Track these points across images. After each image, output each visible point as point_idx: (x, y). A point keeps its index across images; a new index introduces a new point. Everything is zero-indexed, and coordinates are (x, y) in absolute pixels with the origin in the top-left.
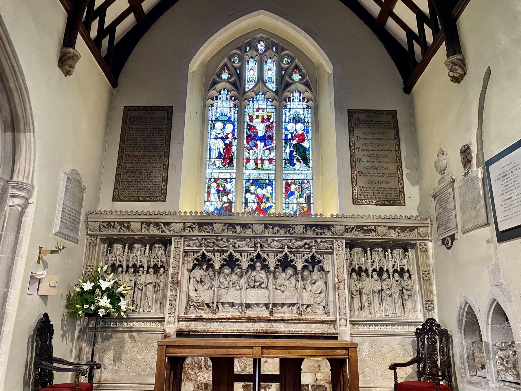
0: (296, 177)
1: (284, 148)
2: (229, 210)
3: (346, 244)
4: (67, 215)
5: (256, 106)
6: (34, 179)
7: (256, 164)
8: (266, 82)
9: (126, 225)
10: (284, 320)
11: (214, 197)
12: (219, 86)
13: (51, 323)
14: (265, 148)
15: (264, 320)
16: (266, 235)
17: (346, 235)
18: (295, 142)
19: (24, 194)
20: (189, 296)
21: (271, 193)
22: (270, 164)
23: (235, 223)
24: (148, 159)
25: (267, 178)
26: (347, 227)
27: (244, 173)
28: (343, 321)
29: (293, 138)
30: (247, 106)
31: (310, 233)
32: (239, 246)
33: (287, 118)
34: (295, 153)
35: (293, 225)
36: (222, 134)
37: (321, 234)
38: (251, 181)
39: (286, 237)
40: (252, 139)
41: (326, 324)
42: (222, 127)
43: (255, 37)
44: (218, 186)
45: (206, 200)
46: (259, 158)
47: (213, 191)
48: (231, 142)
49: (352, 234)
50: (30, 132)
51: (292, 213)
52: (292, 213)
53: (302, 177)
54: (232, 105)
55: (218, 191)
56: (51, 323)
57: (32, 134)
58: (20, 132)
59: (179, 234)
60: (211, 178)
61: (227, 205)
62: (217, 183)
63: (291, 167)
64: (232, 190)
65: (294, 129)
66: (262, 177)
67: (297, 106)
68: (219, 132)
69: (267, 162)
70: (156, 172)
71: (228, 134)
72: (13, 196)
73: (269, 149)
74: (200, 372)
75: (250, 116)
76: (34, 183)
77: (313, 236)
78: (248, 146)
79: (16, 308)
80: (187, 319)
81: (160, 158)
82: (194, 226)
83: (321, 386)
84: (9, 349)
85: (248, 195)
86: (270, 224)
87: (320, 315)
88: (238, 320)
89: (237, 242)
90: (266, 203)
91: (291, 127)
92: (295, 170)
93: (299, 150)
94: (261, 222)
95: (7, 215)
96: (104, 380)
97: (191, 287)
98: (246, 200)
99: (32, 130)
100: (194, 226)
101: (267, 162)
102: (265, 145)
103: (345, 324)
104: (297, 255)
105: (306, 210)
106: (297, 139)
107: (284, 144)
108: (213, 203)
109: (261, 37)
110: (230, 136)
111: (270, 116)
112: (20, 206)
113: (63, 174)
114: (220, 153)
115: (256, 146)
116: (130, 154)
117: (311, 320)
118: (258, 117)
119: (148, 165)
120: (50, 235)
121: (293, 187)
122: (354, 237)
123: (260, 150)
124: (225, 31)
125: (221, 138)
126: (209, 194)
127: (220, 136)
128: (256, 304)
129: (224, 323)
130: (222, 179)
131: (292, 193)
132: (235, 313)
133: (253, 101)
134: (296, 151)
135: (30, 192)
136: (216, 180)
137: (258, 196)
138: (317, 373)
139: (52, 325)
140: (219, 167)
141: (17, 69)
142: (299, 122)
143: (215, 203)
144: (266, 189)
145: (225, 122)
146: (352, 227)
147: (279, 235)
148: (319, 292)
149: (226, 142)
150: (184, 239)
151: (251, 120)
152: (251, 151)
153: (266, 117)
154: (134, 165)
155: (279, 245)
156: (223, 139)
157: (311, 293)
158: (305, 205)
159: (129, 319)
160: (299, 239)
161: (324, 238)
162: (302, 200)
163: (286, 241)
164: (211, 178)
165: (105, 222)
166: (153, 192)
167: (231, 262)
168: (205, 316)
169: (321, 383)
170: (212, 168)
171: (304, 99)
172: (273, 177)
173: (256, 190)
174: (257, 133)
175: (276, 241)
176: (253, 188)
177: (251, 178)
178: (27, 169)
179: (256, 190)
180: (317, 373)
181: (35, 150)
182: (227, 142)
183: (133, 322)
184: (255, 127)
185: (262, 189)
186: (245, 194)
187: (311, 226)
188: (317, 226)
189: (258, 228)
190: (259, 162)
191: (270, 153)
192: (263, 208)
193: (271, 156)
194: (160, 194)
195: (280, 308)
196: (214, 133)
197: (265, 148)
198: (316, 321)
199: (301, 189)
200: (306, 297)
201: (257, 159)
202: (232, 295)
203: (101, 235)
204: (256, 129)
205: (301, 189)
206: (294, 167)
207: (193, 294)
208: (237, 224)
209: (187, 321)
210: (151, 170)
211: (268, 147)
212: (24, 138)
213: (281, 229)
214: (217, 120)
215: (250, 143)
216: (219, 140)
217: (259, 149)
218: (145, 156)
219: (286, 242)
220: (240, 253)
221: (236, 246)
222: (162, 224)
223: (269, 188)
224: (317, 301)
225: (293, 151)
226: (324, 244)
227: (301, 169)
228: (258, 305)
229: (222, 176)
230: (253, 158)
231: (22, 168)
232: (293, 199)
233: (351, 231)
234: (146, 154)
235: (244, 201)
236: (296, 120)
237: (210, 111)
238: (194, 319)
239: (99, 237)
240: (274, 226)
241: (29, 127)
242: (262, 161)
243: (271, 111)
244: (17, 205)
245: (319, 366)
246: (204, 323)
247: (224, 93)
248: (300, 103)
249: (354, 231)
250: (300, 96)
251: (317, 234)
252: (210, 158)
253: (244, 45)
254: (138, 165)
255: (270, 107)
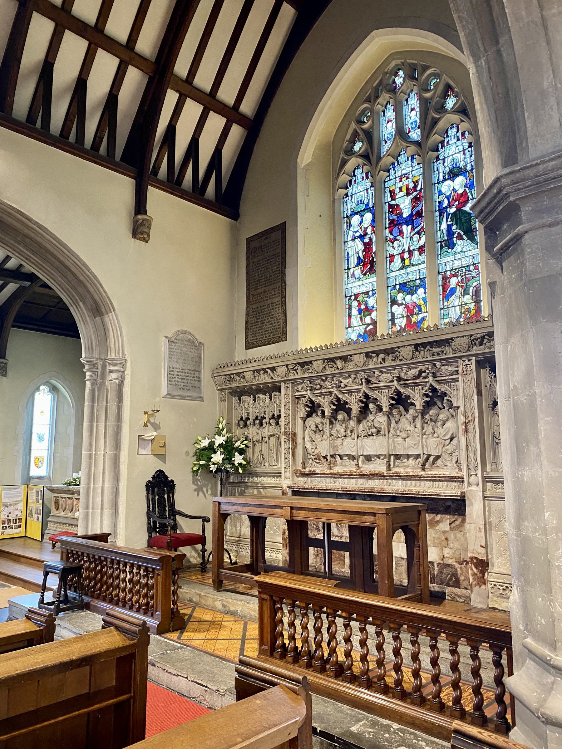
0: (457, 264)
1: (438, 224)
2: (373, 333)
3: (478, 362)
4: (177, 377)
5: (398, 174)
6: (126, 353)
7: (403, 259)
8: (409, 132)
9: (242, 376)
10: (399, 476)
11: (355, 321)
12: (349, 166)
13: (169, 479)
14: (412, 233)
15: (377, 475)
16: (371, 367)
17: (476, 350)
18: (453, 210)
19: (119, 368)
20: (305, 448)
21: (423, 299)
22: (420, 255)
23: (334, 358)
24: (269, 295)
25: (418, 277)
26: (472, 338)
27: (388, 278)
28: (473, 479)
29: (450, 206)
30: (388, 179)
31: (424, 355)
32: (346, 386)
33: (441, 174)
34: (454, 227)
35: (399, 347)
36: (360, 231)
37: (439, 354)
38: (398, 287)
39: (395, 366)
40: (395, 226)
41: (455, 481)
42: (360, 221)
43: (386, 70)
44: (360, 304)
45: (348, 327)
46: (406, 250)
47: (355, 312)
48: (370, 238)
49: (482, 347)
50: (111, 312)
51: (454, 321)
52: (454, 321)
53: (465, 262)
54: (369, 185)
55: (360, 311)
56: (169, 479)
57: (113, 313)
58: (103, 315)
59: (286, 379)
60: (351, 296)
61: (371, 327)
62: (358, 301)
63: (450, 250)
64: (375, 306)
65: (451, 189)
66: (411, 277)
67: (455, 152)
68: (356, 230)
69: (416, 253)
70: (276, 308)
71: (366, 228)
72: (111, 372)
73: (419, 233)
74: (318, 534)
75: (391, 192)
76: (126, 357)
77: (429, 359)
78: (392, 237)
79: (126, 467)
80: (303, 475)
81: (279, 290)
82: (296, 368)
83: (449, 565)
84: (125, 499)
85: (395, 307)
86: (372, 352)
87: (450, 471)
88: (350, 476)
89: (343, 381)
90: (417, 314)
91: (446, 187)
92: (455, 253)
93: (461, 220)
94: (360, 351)
95: (109, 389)
96: (243, 535)
97: (307, 438)
98: (393, 315)
99: (112, 310)
100: (296, 368)
101: (416, 253)
102: (413, 228)
103: (475, 483)
104: (416, 387)
105: (473, 312)
106: (457, 203)
107: (438, 218)
108: (355, 328)
109: (397, 65)
110: (369, 231)
111: (417, 181)
112: (117, 379)
113: (164, 338)
114: (359, 258)
115: (401, 233)
116: (255, 293)
117: (432, 477)
118: (401, 189)
119: (269, 302)
120: (158, 399)
121: (453, 282)
122: (487, 350)
123: (408, 239)
124: (334, 89)
125: (359, 237)
126: (350, 316)
127: (357, 234)
128: (376, 455)
129: (337, 479)
130: (363, 293)
131: (453, 291)
132: (351, 467)
133: (394, 168)
134: (456, 224)
135: (124, 366)
136: (357, 296)
137: (407, 307)
138: (444, 549)
139: (172, 481)
140: (359, 278)
141: (79, 264)
142: (458, 175)
143: (358, 328)
144: (416, 293)
145: (362, 213)
146: (479, 336)
147: (387, 364)
148: (448, 436)
149: (365, 241)
150: (293, 383)
151: (393, 198)
152: (396, 243)
153: (411, 185)
154: (258, 305)
155: (390, 377)
156: (362, 237)
157: (439, 439)
158: (472, 306)
159: (257, 475)
160: (411, 366)
161: (444, 359)
162: (468, 299)
163: (396, 371)
164: (351, 296)
165: (226, 375)
166: (276, 331)
167: (341, 406)
168: (318, 471)
169: (450, 562)
170: (352, 281)
171: (463, 134)
172: (424, 273)
173: (404, 299)
174: (402, 214)
175: (386, 373)
176: (400, 297)
177: (397, 283)
178: (117, 345)
179: (404, 299)
180: (444, 549)
181: (120, 327)
182: (367, 240)
183: (261, 476)
184: (398, 206)
185: (412, 295)
186: (391, 307)
187: (424, 345)
188: (431, 344)
189: (359, 359)
190: (406, 255)
191: (420, 238)
192: (414, 323)
193: (422, 242)
194: (280, 334)
195: (405, 460)
196: (350, 233)
197: (412, 233)
198: (440, 477)
199: (465, 284)
200: (432, 446)
201: (403, 252)
202: (348, 446)
203: (228, 389)
204: (400, 209)
205: (465, 284)
206: (454, 250)
207: (309, 446)
208: (337, 358)
209: (304, 477)
210: (272, 306)
211: (416, 230)
212: (110, 319)
213: (389, 355)
214: (354, 213)
215: (394, 232)
216: (358, 241)
217: (405, 237)
218: (266, 292)
219: (396, 373)
220: (350, 392)
221: (343, 385)
222: (269, 370)
223: (421, 291)
224: (447, 450)
225: (452, 225)
226: (446, 367)
227: (464, 250)
228: (378, 457)
229: (363, 289)
230: (398, 252)
231: (113, 346)
232: (455, 300)
233: (481, 344)
234: (267, 289)
235: (390, 318)
236: (452, 175)
237: (345, 204)
238: (308, 474)
239: (474, 358)
240: (377, 353)
241: (110, 308)
242: (410, 252)
243: (417, 172)
244: (115, 379)
245: (447, 539)
246: (320, 479)
247: (358, 172)
248: (459, 143)
249: (485, 341)
250: (457, 132)
251: (433, 355)
252: (348, 269)
253: (380, 87)
254: (263, 303)
255: (417, 167)
